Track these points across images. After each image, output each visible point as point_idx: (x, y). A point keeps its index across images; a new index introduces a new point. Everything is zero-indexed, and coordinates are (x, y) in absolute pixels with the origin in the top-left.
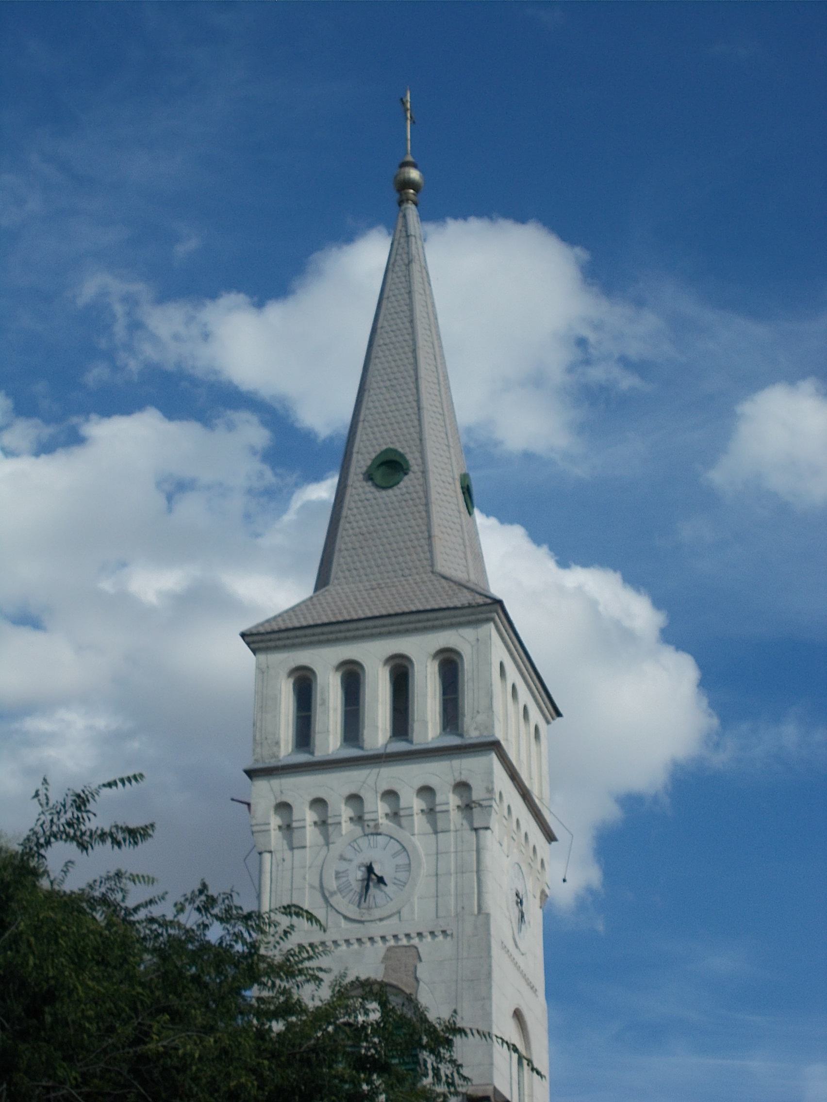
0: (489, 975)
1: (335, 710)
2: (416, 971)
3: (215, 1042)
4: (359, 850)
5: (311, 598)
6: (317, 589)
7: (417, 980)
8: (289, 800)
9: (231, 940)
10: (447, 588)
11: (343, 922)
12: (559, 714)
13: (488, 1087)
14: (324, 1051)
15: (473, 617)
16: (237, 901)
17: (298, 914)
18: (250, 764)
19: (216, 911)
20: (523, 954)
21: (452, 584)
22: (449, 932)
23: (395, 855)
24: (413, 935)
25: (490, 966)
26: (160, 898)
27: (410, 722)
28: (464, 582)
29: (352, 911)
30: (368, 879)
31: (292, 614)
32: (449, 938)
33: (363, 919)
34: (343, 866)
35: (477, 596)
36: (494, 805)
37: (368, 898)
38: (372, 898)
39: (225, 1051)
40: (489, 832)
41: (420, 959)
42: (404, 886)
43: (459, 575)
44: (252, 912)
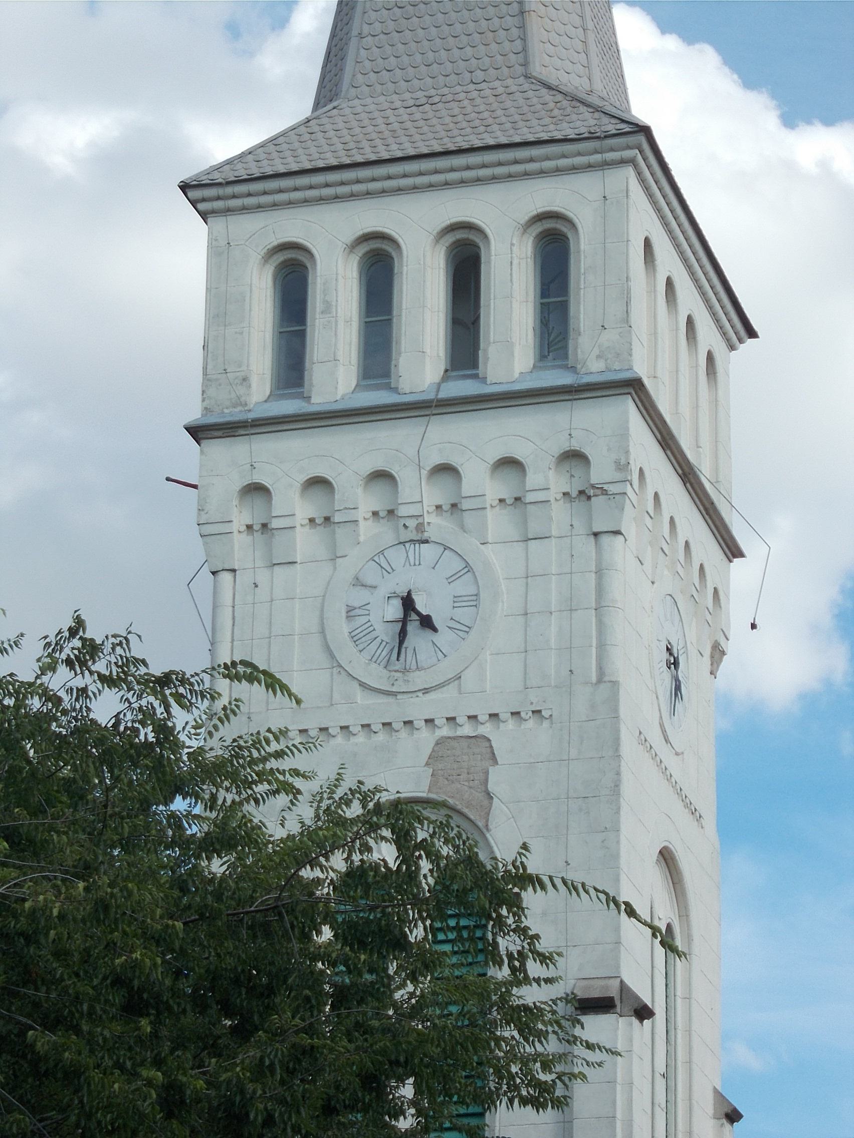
0: (616, 788)
1: (348, 322)
2: (486, 781)
3: (87, 889)
4: (390, 570)
5: (308, 121)
6: (317, 105)
7: (489, 796)
8: (266, 481)
9: (133, 721)
10: (551, 105)
11: (360, 696)
12: (752, 333)
13: (612, 981)
14: (292, 911)
15: (597, 158)
16: (137, 651)
17: (251, 679)
18: (194, 415)
19: (100, 666)
20: (677, 754)
21: (559, 97)
22: (545, 713)
23: (451, 579)
24: (483, 718)
25: (618, 774)
26: (12, 643)
27: (482, 345)
28: (583, 96)
29: (376, 676)
30: (404, 622)
31: (271, 148)
32: (546, 724)
33: (394, 689)
34: (358, 597)
35: (606, 120)
36: (629, 490)
37: (403, 650)
38: (410, 653)
39: (103, 906)
40: (620, 538)
41: (494, 759)
42: (467, 632)
43: (575, 82)
44: (172, 672)
